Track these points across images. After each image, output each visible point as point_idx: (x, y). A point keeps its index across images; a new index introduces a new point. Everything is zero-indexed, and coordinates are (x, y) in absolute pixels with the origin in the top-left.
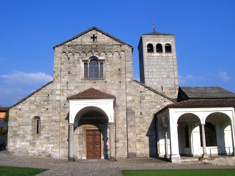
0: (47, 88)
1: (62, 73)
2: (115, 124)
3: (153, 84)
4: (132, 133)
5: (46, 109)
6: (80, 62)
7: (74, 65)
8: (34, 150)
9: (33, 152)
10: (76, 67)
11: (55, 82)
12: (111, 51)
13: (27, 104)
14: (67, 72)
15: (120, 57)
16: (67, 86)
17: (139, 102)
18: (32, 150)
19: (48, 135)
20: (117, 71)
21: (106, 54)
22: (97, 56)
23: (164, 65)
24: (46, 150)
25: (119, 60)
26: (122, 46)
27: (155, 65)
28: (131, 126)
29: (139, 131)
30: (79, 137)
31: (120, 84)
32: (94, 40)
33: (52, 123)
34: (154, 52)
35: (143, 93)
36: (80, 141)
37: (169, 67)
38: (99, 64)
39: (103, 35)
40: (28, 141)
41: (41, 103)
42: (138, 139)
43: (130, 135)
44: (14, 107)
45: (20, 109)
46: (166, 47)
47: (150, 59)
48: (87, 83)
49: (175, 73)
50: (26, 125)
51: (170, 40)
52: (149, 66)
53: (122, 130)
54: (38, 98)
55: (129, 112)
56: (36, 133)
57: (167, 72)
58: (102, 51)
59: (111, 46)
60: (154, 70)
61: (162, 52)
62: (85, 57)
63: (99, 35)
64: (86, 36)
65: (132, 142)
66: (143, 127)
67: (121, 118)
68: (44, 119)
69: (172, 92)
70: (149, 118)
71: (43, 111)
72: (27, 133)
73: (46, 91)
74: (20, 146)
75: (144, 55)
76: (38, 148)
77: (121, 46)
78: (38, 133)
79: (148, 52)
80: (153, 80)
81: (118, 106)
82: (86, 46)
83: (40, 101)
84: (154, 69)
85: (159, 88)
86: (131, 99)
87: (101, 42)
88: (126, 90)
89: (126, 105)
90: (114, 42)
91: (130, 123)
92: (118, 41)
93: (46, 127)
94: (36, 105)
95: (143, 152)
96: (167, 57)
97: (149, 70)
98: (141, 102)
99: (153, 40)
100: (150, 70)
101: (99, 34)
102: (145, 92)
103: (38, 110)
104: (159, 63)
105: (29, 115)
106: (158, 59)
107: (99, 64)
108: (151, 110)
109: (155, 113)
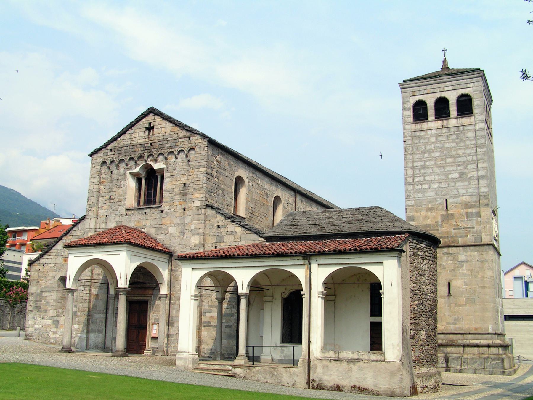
0: (78, 227)
1: (101, 199)
3: (424, 196)
7: (118, 184)
10: (120, 186)
12: (173, 150)
15: (189, 161)
18: (54, 333)
20: (181, 189)
21: (166, 159)
23: (451, 148)
25: (185, 167)
26: (191, 138)
27: (430, 152)
29: (210, 304)
34: (430, 118)
35: (222, 229)
37: (465, 153)
45: (44, 264)
47: (419, 138)
49: (480, 166)
50: (49, 292)
51: (469, 85)
52: (417, 154)
57: (459, 165)
58: (159, 153)
60: (427, 163)
61: (449, 116)
62: (134, 167)
69: (472, 213)
74: (40, 326)
82: (135, 147)
86: (197, 242)
96: (461, 128)
97: (415, 164)
99: (426, 92)
100: (419, 164)
102: (225, 227)
104: (439, 145)
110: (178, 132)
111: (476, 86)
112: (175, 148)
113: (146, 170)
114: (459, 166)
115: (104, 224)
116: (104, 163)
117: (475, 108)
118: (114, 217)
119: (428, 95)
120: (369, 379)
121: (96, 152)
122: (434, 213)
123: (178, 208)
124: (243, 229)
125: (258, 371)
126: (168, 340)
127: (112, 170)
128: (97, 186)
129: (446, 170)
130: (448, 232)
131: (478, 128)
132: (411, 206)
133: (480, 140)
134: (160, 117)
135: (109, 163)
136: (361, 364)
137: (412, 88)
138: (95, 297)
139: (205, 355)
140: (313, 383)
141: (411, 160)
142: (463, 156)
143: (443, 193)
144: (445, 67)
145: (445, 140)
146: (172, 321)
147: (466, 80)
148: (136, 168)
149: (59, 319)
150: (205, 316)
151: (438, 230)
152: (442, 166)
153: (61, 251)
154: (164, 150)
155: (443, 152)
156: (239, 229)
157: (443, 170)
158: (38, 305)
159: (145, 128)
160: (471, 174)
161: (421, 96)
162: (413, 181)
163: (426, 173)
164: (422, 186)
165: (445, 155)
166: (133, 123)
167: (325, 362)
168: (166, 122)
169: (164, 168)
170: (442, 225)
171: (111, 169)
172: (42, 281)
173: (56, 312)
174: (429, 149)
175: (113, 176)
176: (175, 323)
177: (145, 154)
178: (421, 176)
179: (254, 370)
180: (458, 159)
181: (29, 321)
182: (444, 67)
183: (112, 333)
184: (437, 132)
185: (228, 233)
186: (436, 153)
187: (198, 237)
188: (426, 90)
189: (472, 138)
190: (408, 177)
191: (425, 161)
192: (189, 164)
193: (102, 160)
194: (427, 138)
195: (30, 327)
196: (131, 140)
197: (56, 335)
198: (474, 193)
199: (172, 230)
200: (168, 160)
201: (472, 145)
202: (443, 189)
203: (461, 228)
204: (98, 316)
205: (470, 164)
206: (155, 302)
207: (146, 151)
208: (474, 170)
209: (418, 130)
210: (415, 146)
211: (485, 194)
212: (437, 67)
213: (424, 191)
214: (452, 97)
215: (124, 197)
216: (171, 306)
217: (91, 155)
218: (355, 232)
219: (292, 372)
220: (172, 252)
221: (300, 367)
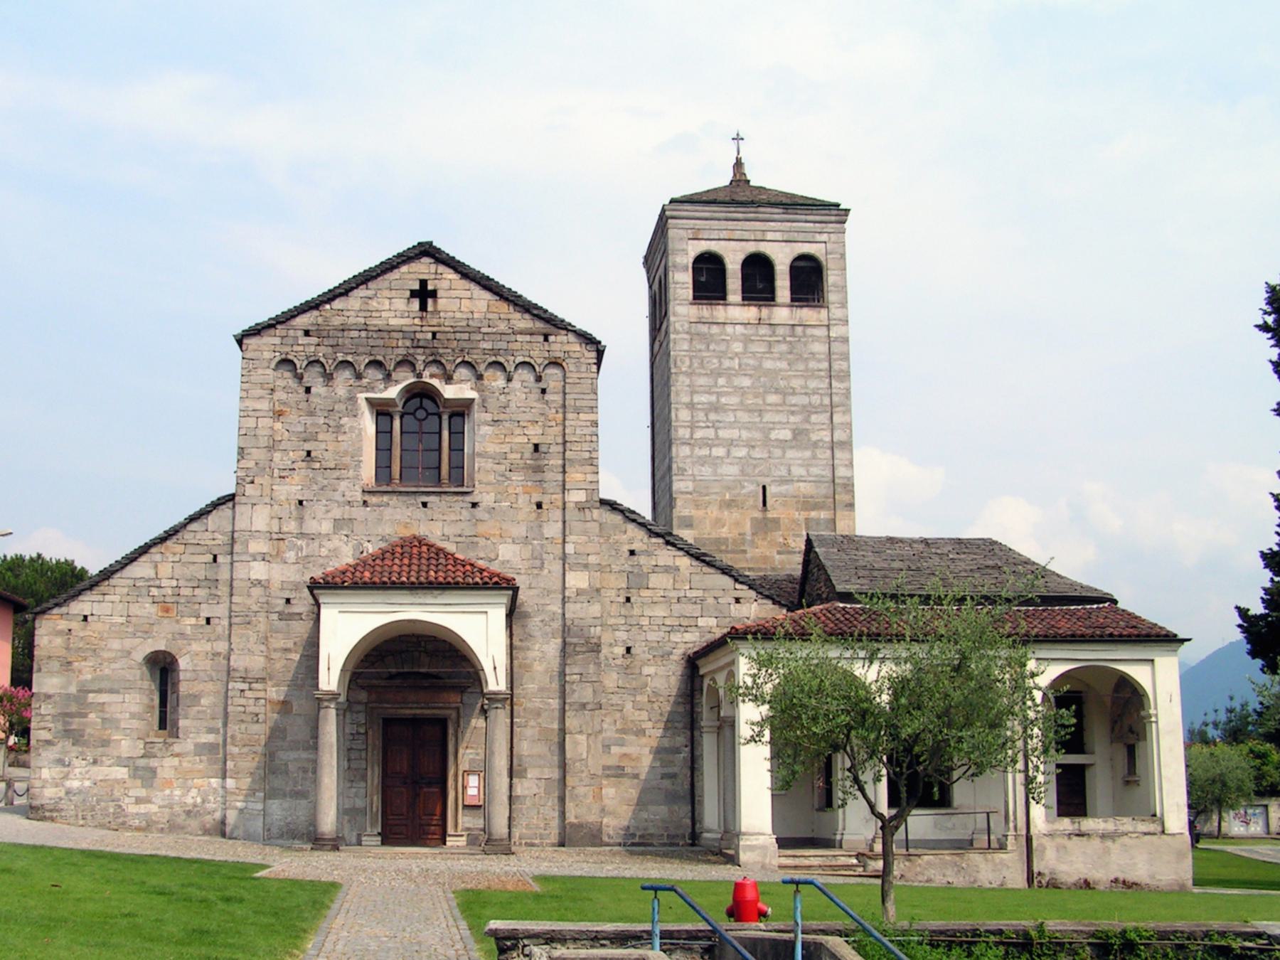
0: (207, 524)
2: (509, 699)
3: (715, 473)
7: (331, 423)
8: (148, 801)
9: (143, 808)
10: (339, 429)
11: (243, 499)
12: (501, 359)
13: (117, 598)
15: (544, 391)
16: (301, 519)
17: (622, 599)
18: (139, 801)
20: (527, 455)
21: (480, 377)
22: (435, 382)
23: (776, 372)
24: (203, 802)
25: (535, 404)
26: (552, 338)
27: (729, 374)
28: (583, 706)
29: (619, 726)
31: (539, 516)
32: (423, 307)
35: (642, 560)
36: (354, 765)
37: (806, 387)
38: (445, 417)
40: (120, 762)
41: (184, 592)
42: (612, 761)
43: (578, 746)
46: (793, 268)
50: (111, 691)
51: (819, 237)
52: (700, 374)
53: (540, 720)
55: (575, 645)
56: (156, 727)
57: (793, 413)
59: (504, 337)
60: (723, 400)
61: (773, 299)
64: (386, 284)
67: (538, 667)
68: (196, 665)
72: (117, 728)
73: (205, 538)
74: (87, 783)
75: (675, 315)
76: (167, 792)
77: (546, 339)
78: (163, 724)
79: (695, 298)
80: (719, 452)
81: (526, 616)
82: (385, 335)
83: (174, 583)
85: (748, 495)
87: (458, 315)
88: (564, 542)
89: (560, 611)
90: (518, 315)
91: (576, 695)
92: (535, 312)
93: (203, 701)
94: (156, 600)
96: (799, 330)
97: (697, 399)
98: (628, 599)
99: (724, 235)
100: (704, 398)
102: (649, 554)
103: (166, 621)
104: (751, 362)
105: (128, 643)
106: (747, 340)
107: (445, 417)
108: (676, 637)
109: (691, 652)
110: (510, 316)
112: (506, 355)
115: (293, 523)
119: (727, 242)
120: (1140, 866)
121: (256, 331)
122: (736, 515)
123: (523, 500)
124: (695, 563)
125: (929, 863)
127: (308, 385)
129: (764, 420)
130: (765, 559)
132: (687, 493)
134: (451, 271)
135: (304, 366)
136: (1125, 839)
138: (278, 708)
140: (1039, 878)
143: (757, 472)
144: (739, 179)
145: (764, 353)
146: (520, 765)
147: (812, 225)
148: (386, 388)
151: (744, 552)
154: (475, 357)
156: (684, 562)
157: (758, 420)
158: (74, 727)
161: (714, 242)
162: (692, 438)
165: (764, 386)
167: (1059, 840)
168: (473, 286)
169: (474, 400)
170: (753, 541)
171: (305, 380)
172: (83, 663)
173: (142, 746)
174: (729, 369)
176: (529, 771)
177: (419, 357)
178: (708, 427)
179: (920, 861)
180: (791, 397)
181: (43, 770)
184: (746, 332)
185: (657, 569)
186: (743, 377)
191: (719, 394)
193: (277, 354)
194: (725, 343)
195: (48, 785)
196: (369, 314)
197: (149, 806)
200: (486, 382)
201: (820, 370)
203: (795, 552)
204: (293, 755)
205: (816, 413)
206: (470, 721)
207: (420, 351)
208: (824, 427)
210: (695, 357)
211: (845, 481)
212: (723, 178)
213: (715, 462)
219: (998, 861)
221: (1012, 851)
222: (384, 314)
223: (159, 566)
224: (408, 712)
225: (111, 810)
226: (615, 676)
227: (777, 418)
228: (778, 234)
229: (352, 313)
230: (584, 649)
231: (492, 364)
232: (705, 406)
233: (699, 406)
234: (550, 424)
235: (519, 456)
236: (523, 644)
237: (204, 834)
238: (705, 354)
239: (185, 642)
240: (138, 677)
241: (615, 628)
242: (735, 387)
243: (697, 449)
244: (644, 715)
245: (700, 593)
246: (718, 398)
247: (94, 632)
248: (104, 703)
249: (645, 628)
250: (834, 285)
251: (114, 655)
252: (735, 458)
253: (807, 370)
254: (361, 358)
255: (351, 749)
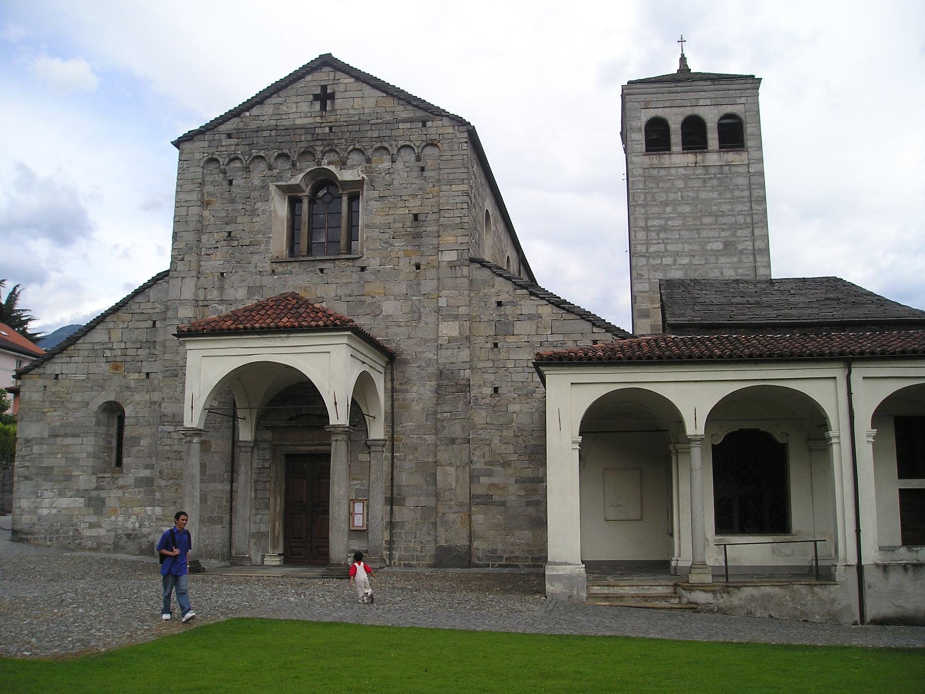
1: (205, 237)
4: (454, 470)
5: (144, 376)
6: (270, 194)
7: (248, 208)
8: (98, 526)
9: (94, 532)
10: (254, 212)
12: (386, 145)
13: (80, 359)
14: (221, 235)
15: (423, 169)
16: (222, 289)
17: (490, 345)
18: (92, 526)
19: (147, 473)
20: (408, 224)
21: (369, 161)
22: (332, 168)
24: (140, 527)
25: (415, 181)
26: (429, 124)
28: (453, 441)
30: (256, 482)
32: (323, 107)
33: (160, 429)
34: (674, 149)
35: (508, 309)
39: (360, 84)
40: (79, 493)
41: (131, 352)
44: (36, 370)
45: (57, 375)
46: (720, 126)
47: (657, 180)
48: (291, 273)
50: (75, 436)
51: (738, 101)
52: (652, 205)
53: (417, 455)
54: (116, 335)
57: (723, 230)
58: (351, 148)
61: (706, 148)
62: (289, 175)
63: (341, 88)
64: (294, 92)
65: (453, 503)
66: (503, 447)
67: (416, 408)
68: (137, 412)
70: (526, 408)
71: (133, 382)
73: (147, 307)
74: (54, 511)
76: (113, 518)
77: (424, 125)
79: (647, 151)
80: (668, 261)
83: (123, 345)
84: (674, 218)
86: (455, 333)
87: (352, 112)
90: (401, 108)
91: (446, 431)
95: (500, 546)
98: (496, 345)
99: (668, 104)
100: (656, 223)
101: (346, 81)
102: (513, 303)
104: (691, 194)
106: (686, 178)
110: (394, 109)
111: (750, 104)
113: (313, 182)
114: (723, 231)
115: (215, 292)
116: (212, 160)
117: (749, 139)
118: (242, 276)
121: (190, 137)
124: (556, 310)
126: (391, 535)
127: (231, 178)
128: (195, 210)
131: (753, 171)
132: (645, 292)
133: (757, 191)
137: (644, 96)
139: (481, 563)
141: (643, 216)
142: (729, 215)
145: (700, 187)
149: (105, 495)
150: (479, 483)
152: (695, 230)
153: (104, 347)
154: (364, 144)
155: (697, 205)
156: (546, 310)
159: (312, 96)
160: (743, 245)
163: (668, 239)
164: (661, 259)
166: (284, 84)
174: (675, 200)
175: (235, 190)
178: (659, 243)
180: (721, 218)
182: (682, 68)
183: (250, 523)
184: (686, 173)
185: (521, 318)
187: (457, 323)
188: (668, 102)
189: (745, 187)
190: (639, 244)
191: (667, 219)
192: (424, 175)
193: (205, 155)
198: (748, 276)
199: (389, 307)
200: (374, 165)
201: (744, 197)
202: (697, 267)
205: (740, 229)
208: (747, 239)
209: (655, 166)
212: (673, 68)
214: (711, 117)
215: (267, 235)
216: (395, 464)
217: (177, 144)
218: (862, 319)
220: (394, 353)
222: (291, 116)
223: (112, 332)
224: (305, 448)
225: (71, 534)
226: (484, 413)
227: (711, 234)
228: (707, 100)
229: (266, 117)
230: (454, 390)
231: (378, 149)
232: (657, 228)
233: (652, 229)
234: (428, 196)
235: (401, 225)
236: (403, 387)
237: (140, 554)
238: (655, 190)
239: (129, 393)
240: (94, 424)
241: (484, 371)
242: (680, 213)
243: (651, 260)
244: (510, 449)
245: (560, 337)
246: (666, 222)
247: (62, 388)
248: (68, 445)
249: (511, 370)
250: (752, 134)
251: (76, 406)
252: (680, 264)
253: (732, 198)
254: (271, 153)
255: (258, 481)
